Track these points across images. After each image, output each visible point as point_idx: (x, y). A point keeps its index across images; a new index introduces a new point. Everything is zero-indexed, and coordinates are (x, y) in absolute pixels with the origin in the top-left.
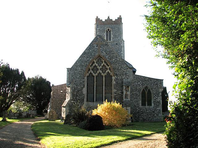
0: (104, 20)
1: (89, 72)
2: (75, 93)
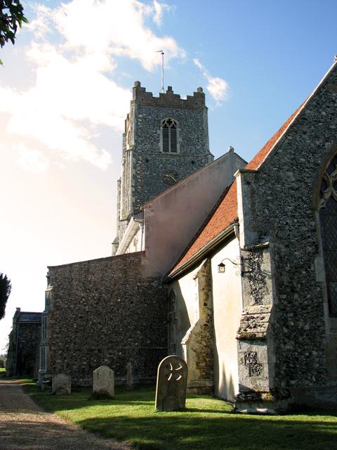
0: (156, 95)
1: (327, 196)
2: (285, 279)
